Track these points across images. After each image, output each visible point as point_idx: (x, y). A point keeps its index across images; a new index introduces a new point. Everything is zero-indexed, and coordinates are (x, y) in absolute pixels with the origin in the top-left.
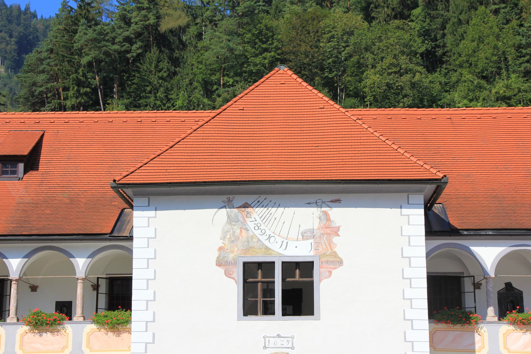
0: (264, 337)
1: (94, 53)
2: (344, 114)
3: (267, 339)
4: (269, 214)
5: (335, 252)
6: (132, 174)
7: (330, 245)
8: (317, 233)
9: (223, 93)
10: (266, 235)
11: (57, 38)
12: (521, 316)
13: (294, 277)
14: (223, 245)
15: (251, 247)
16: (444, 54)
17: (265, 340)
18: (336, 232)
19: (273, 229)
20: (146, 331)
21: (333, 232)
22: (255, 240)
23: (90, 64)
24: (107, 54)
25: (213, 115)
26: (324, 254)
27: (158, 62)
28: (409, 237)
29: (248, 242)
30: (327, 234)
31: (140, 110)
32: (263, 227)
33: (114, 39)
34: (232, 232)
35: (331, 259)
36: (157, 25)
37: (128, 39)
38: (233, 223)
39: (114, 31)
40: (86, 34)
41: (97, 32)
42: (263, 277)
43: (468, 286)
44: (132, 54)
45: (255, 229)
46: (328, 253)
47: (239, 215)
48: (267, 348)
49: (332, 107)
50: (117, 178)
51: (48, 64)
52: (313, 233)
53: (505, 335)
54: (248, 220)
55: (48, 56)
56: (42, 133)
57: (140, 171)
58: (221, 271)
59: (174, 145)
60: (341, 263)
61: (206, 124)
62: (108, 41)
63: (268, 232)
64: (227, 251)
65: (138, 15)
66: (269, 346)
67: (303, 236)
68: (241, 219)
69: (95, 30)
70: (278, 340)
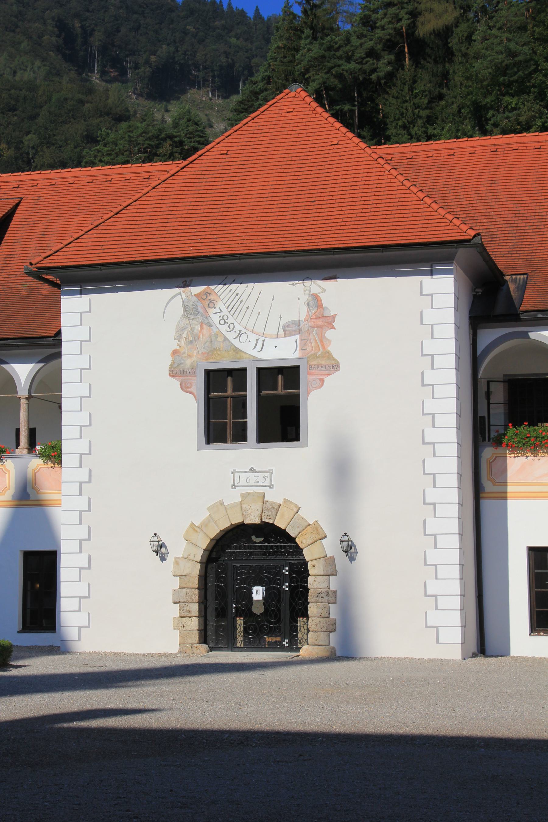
0: (232, 472)
2: (363, 151)
3: (237, 475)
4: (239, 302)
5: (329, 352)
6: (57, 254)
7: (321, 341)
8: (305, 326)
9: (501, 121)
10: (235, 332)
11: (276, 61)
13: (276, 388)
14: (178, 348)
15: (214, 349)
17: (234, 477)
19: (244, 323)
20: (81, 466)
21: (326, 324)
22: (220, 339)
24: (340, 77)
25: (182, 166)
26: (313, 355)
28: (432, 325)
29: (211, 342)
30: (318, 327)
31: (160, 161)
32: (230, 321)
34: (189, 329)
35: (323, 362)
36: (413, 26)
37: (372, 53)
38: (191, 316)
39: (349, 43)
40: (309, 50)
41: (324, 46)
42: (234, 390)
44: (379, 74)
45: (220, 324)
46: (320, 353)
47: (199, 304)
48: (237, 486)
49: (349, 141)
50: (33, 262)
52: (299, 326)
54: (211, 311)
55: (264, 88)
56: (17, 201)
57: (68, 249)
58: (176, 383)
59: (121, 211)
60: (336, 366)
61: (171, 178)
62: (340, 58)
63: (238, 328)
64: (183, 356)
65: (386, 14)
66: (239, 485)
67: (285, 331)
68: (201, 311)
70: (252, 475)
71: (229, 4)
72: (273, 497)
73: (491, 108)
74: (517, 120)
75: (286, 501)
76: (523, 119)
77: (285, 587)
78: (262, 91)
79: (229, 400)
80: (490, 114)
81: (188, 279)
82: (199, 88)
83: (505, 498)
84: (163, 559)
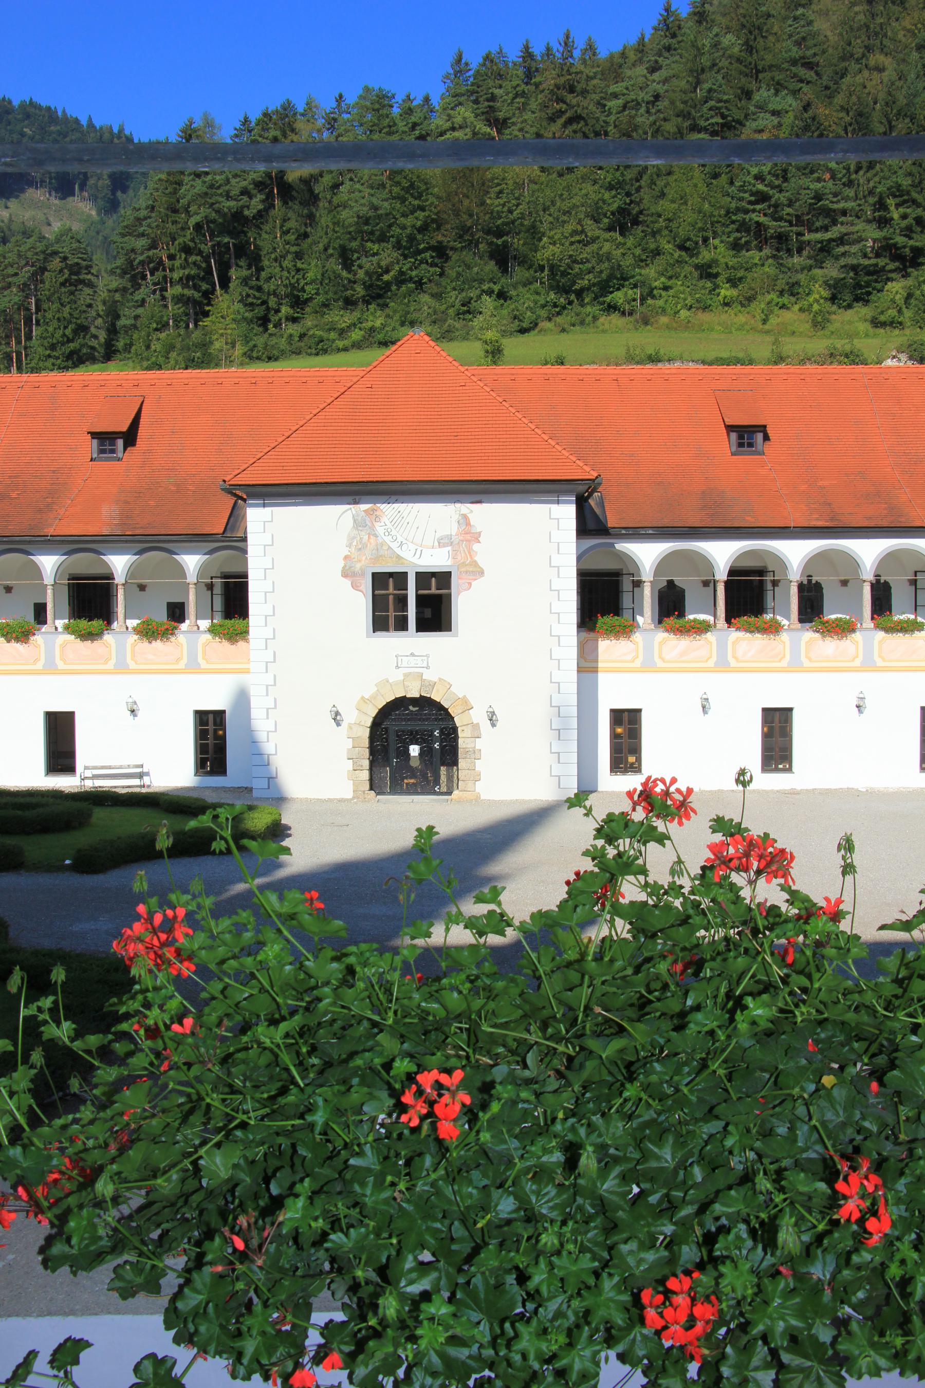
1: (204, 211)
12: (681, 622)
16: (641, 212)
18: (476, 537)
22: (385, 548)
23: (198, 227)
27: (285, 221)
33: (228, 192)
37: (244, 192)
43: (626, 585)
47: (367, 519)
51: (149, 226)
53: (661, 644)
54: (377, 525)
58: (347, 583)
60: (482, 573)
62: (221, 195)
63: (400, 539)
69: (205, 182)
71: (64, 111)
72: (429, 676)
73: (356, 251)
74: (378, 264)
75: (440, 679)
76: (383, 264)
77: (436, 746)
78: (145, 218)
79: (391, 597)
80: (356, 255)
81: (357, 498)
82: (37, 188)
83: (597, 672)
84: (338, 725)
